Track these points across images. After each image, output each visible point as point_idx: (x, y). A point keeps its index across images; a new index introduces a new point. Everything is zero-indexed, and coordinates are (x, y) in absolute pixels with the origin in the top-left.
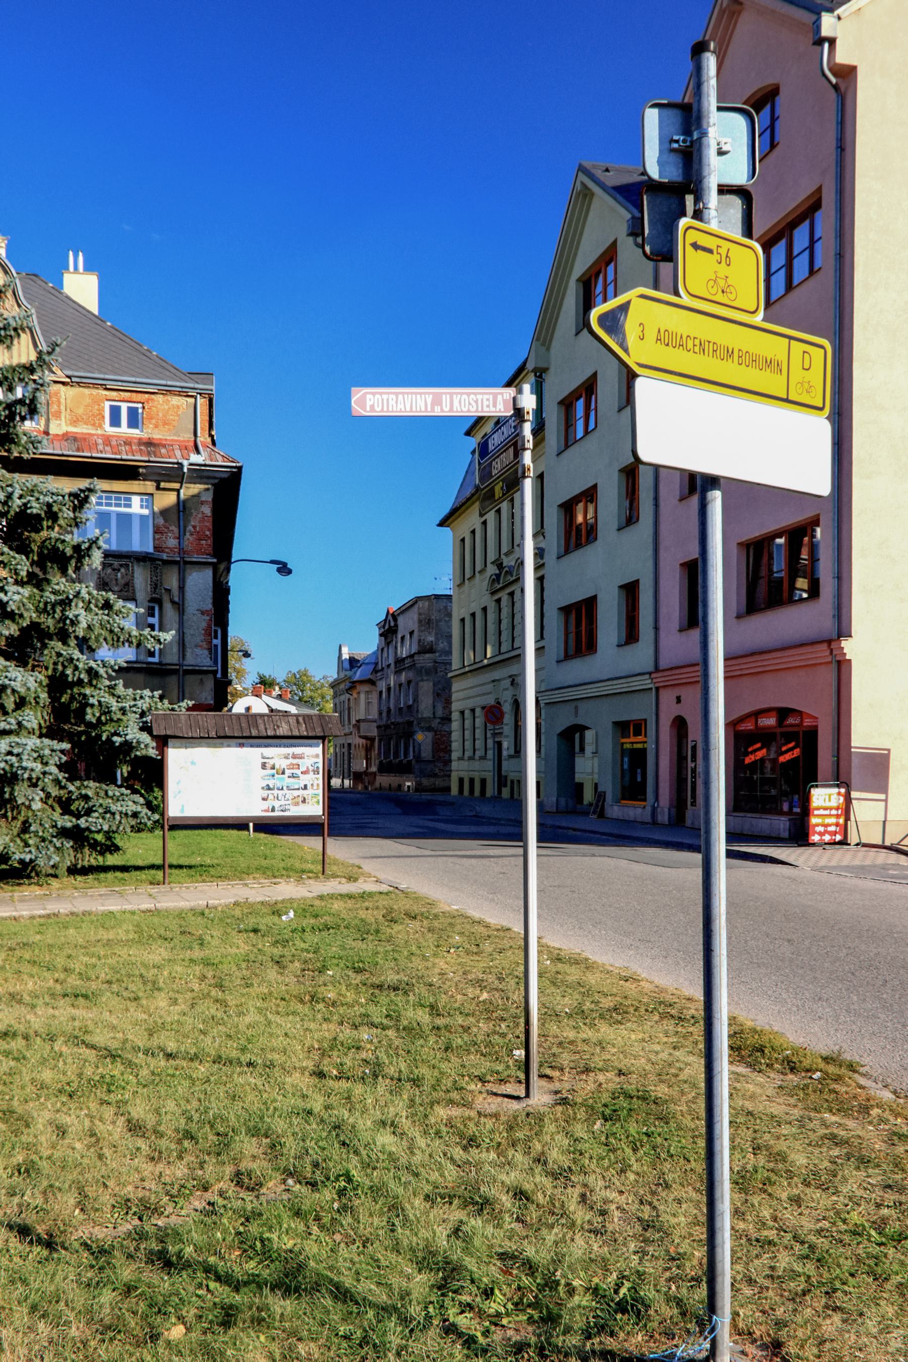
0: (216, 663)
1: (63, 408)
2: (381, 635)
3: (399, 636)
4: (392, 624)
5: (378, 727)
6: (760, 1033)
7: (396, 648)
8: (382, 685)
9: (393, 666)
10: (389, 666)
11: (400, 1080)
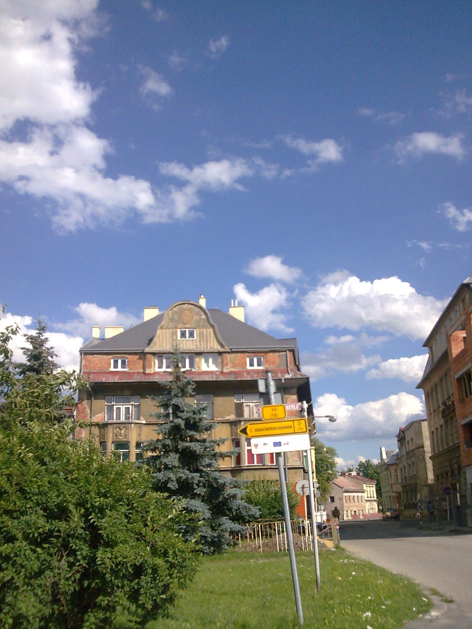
0: (303, 463)
1: (229, 361)
2: (398, 441)
3: (406, 442)
4: (403, 435)
5: (402, 486)
6: (401, 575)
7: (406, 447)
8: (401, 466)
9: (405, 456)
10: (403, 456)
11: (78, 470)
